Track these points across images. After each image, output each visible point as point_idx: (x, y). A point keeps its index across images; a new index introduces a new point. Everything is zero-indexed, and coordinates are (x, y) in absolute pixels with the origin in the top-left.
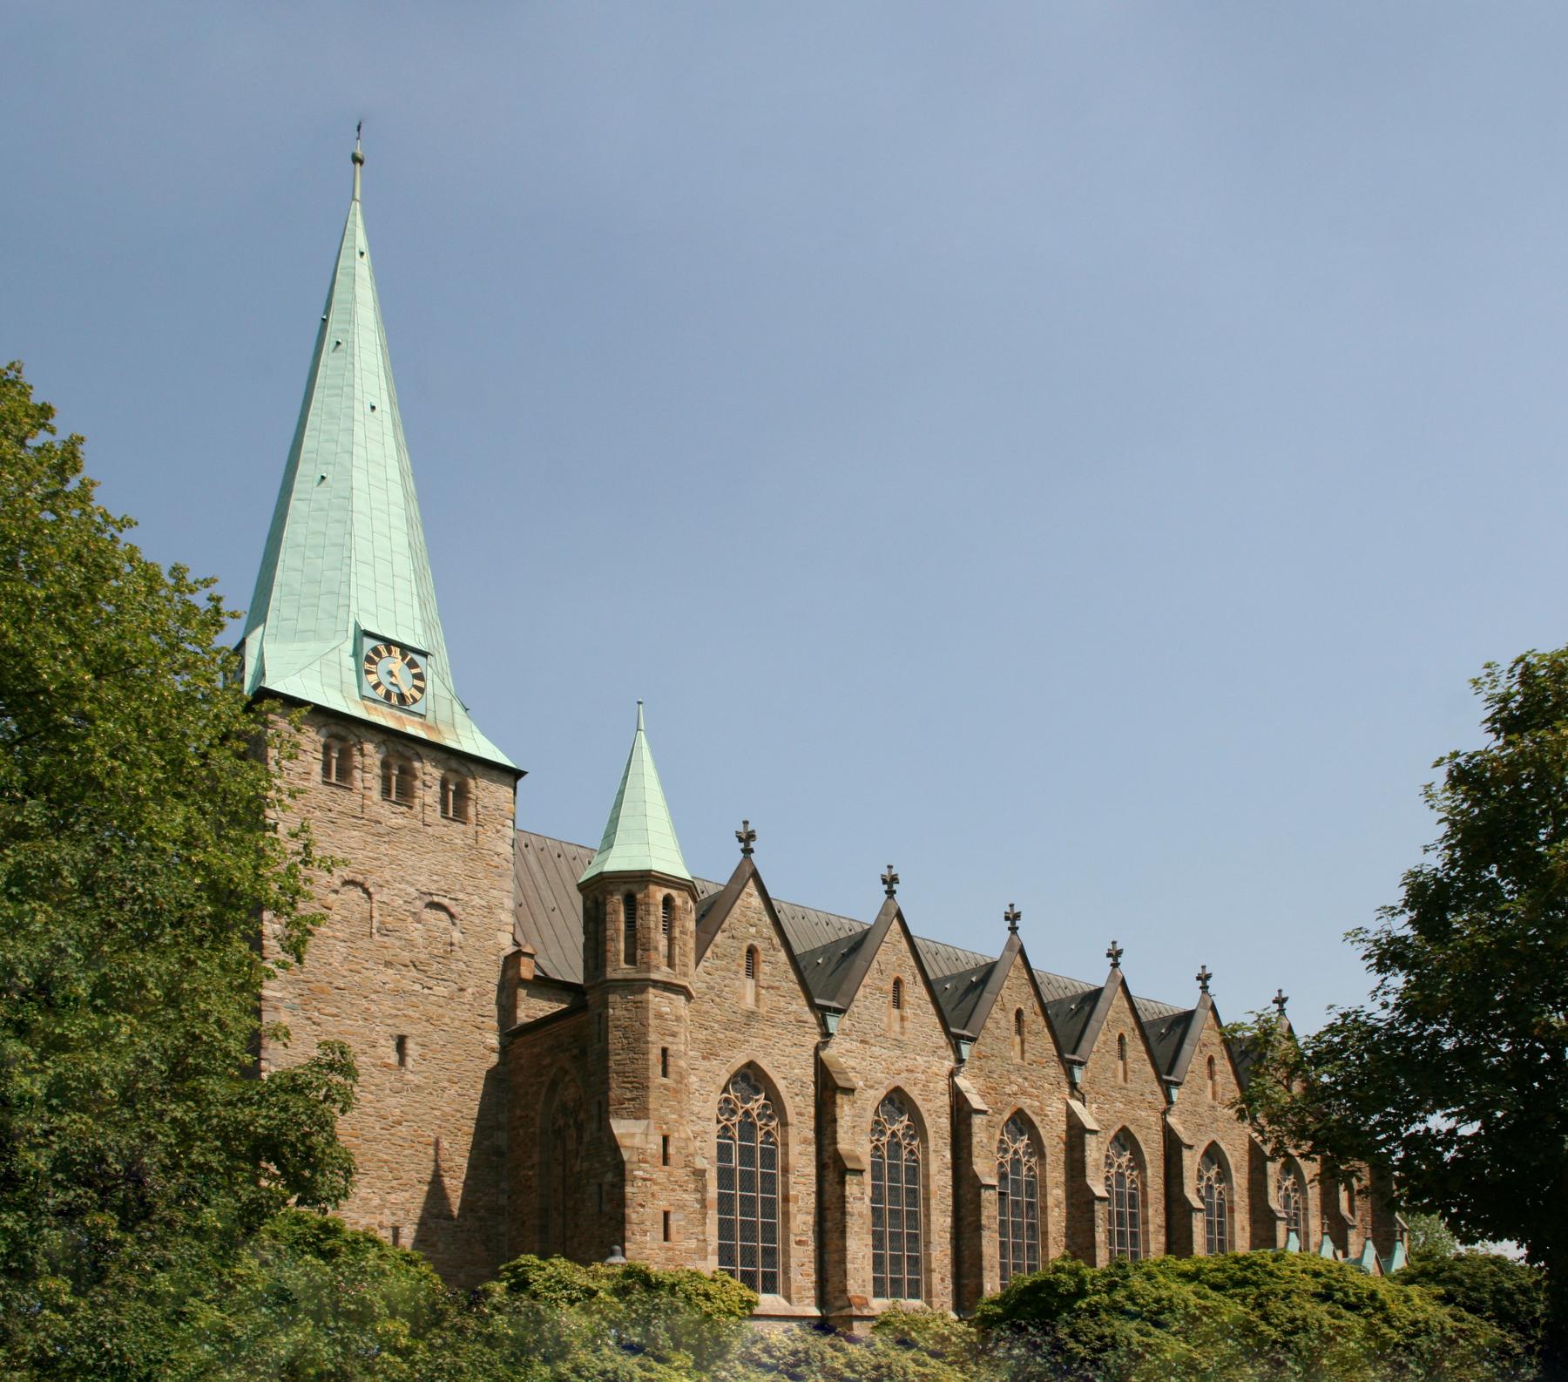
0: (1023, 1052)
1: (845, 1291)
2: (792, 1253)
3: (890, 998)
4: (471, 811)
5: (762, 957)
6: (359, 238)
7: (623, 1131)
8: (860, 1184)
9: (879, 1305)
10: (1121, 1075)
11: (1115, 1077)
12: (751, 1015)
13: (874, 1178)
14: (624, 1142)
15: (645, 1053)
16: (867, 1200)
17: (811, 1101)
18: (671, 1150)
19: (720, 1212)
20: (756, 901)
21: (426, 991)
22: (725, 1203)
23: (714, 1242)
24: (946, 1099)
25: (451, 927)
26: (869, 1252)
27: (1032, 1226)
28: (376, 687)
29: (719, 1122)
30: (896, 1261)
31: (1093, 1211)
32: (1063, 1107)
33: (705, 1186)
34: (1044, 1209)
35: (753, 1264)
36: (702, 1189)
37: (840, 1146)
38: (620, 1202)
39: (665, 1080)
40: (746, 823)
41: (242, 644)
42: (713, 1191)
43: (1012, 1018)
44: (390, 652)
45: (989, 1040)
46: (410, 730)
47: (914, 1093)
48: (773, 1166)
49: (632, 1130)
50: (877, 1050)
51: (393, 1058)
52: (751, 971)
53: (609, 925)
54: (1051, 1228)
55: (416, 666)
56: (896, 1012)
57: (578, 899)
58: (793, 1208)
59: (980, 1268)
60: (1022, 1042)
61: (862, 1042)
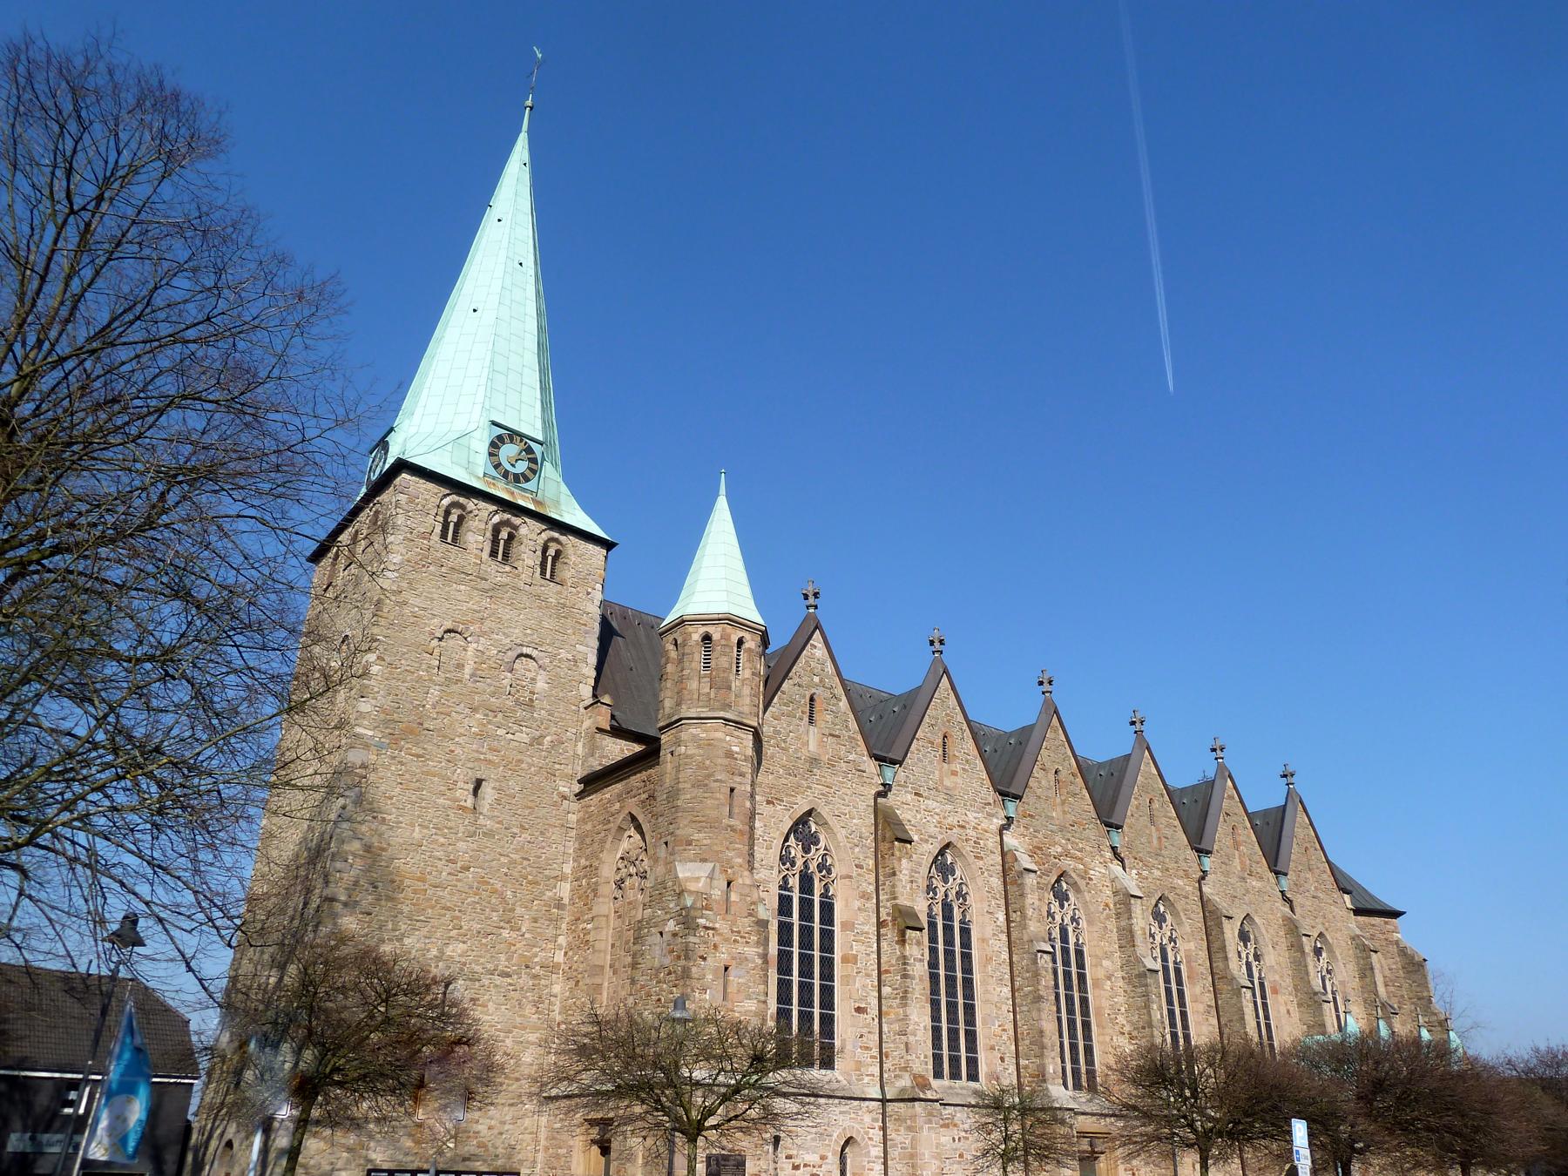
6: (520, 152)
7: (688, 874)
8: (919, 943)
12: (814, 761)
31: (1290, 1133)
33: (767, 939)
36: (765, 942)
46: (521, 502)
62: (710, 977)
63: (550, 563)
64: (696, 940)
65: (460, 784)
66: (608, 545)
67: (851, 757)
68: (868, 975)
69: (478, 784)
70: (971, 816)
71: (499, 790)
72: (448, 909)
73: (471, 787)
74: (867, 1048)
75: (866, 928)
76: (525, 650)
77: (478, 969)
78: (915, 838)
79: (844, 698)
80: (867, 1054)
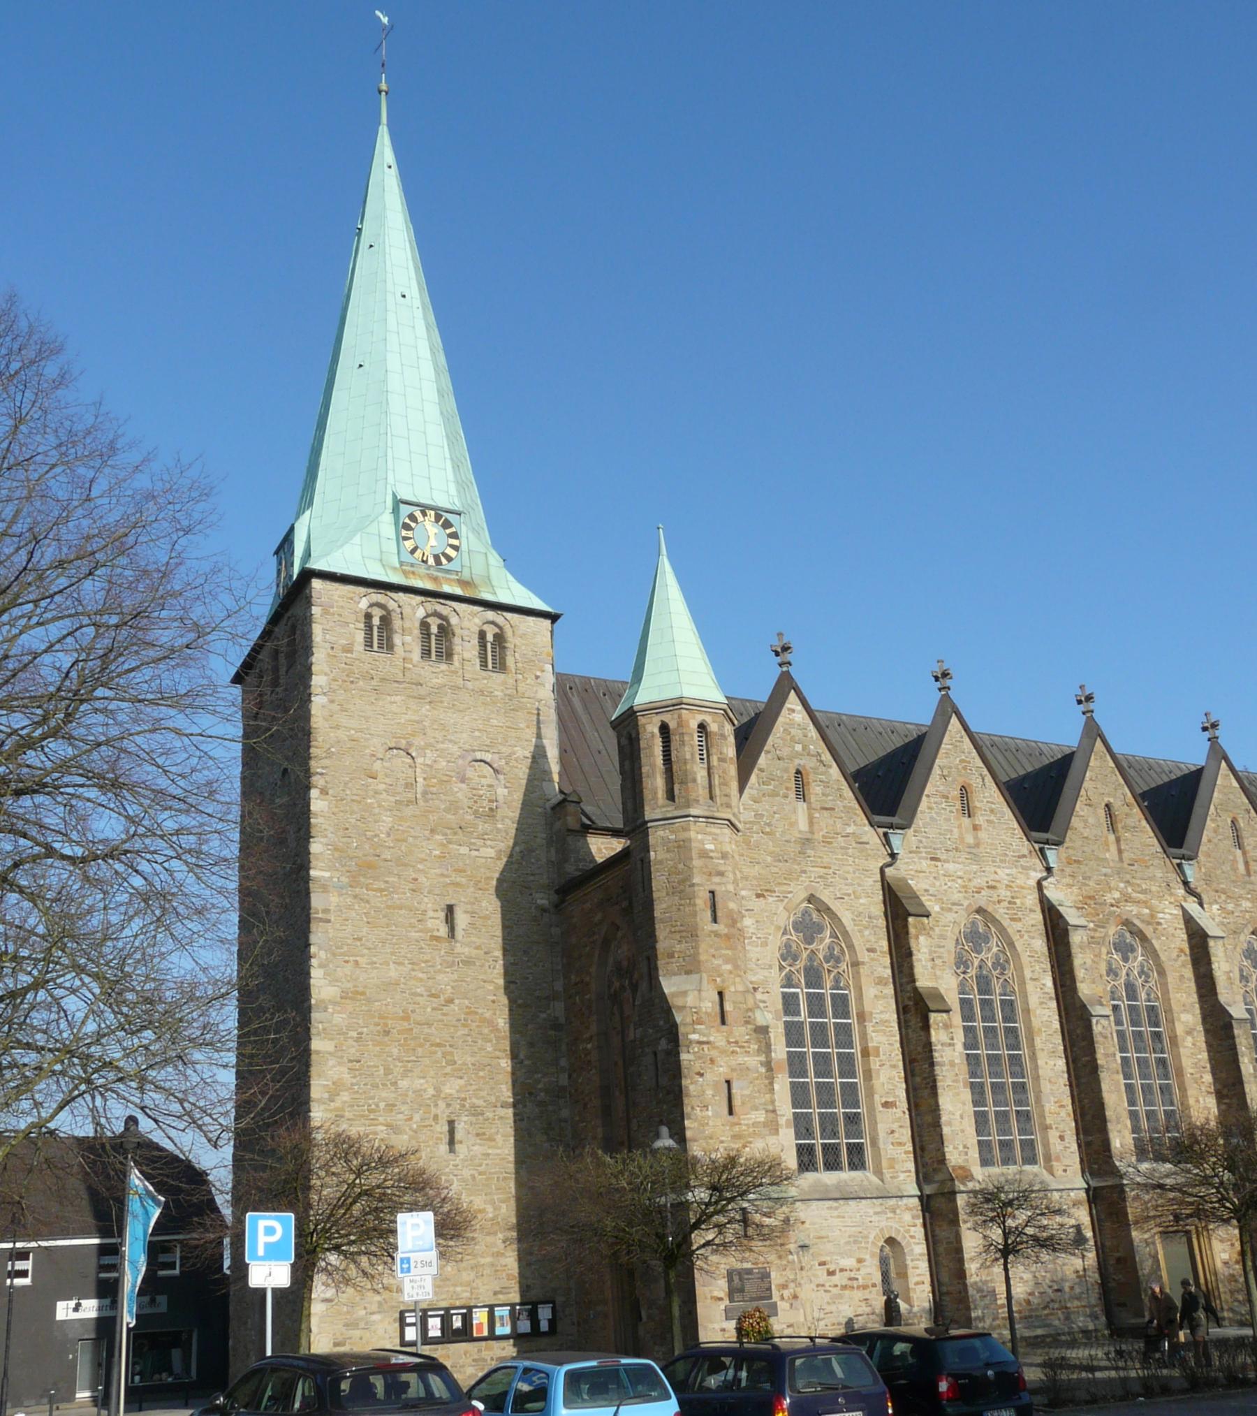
0: (1120, 851)
1: (942, 1160)
2: (879, 1117)
3: (958, 805)
4: (510, 661)
5: (811, 777)
7: (673, 989)
8: (947, 1026)
9: (982, 1176)
10: (1241, 868)
11: (1235, 870)
12: (806, 842)
13: (964, 1019)
14: (675, 1002)
15: (692, 897)
16: (959, 1047)
17: (883, 933)
18: (728, 1007)
19: (792, 1075)
20: (800, 716)
21: (475, 853)
22: (796, 1065)
23: (786, 1110)
24: (1038, 917)
25: (495, 782)
26: (970, 1109)
27: (1162, 1062)
28: (413, 551)
29: (781, 968)
30: (1002, 1117)
31: (1233, 1037)
32: (1178, 912)
33: (768, 1046)
34: (1174, 1040)
35: (835, 1134)
36: (767, 1048)
37: (918, 984)
38: (676, 1072)
39: (715, 927)
40: (780, 634)
41: (292, 529)
42: (780, 1051)
43: (1102, 813)
44: (424, 514)
45: (1079, 843)
47: (1001, 913)
48: (846, 1015)
49: (683, 988)
50: (951, 867)
51: (443, 930)
52: (801, 792)
53: (644, 760)
54: (1187, 1064)
55: (451, 526)
56: (966, 821)
57: (612, 734)
58: (874, 1063)
59: (1104, 1120)
60: (1118, 840)
61: (932, 859)
62: (709, 1092)
63: (495, 651)
64: (691, 1057)
65: (431, 914)
66: (554, 618)
67: (850, 830)
68: (894, 1066)
69: (450, 910)
70: (1003, 874)
71: (472, 914)
72: (439, 1045)
73: (442, 915)
74: (900, 1144)
75: (885, 1017)
76: (479, 756)
77: (480, 1102)
78: (934, 908)
79: (835, 765)
80: (901, 1149)
